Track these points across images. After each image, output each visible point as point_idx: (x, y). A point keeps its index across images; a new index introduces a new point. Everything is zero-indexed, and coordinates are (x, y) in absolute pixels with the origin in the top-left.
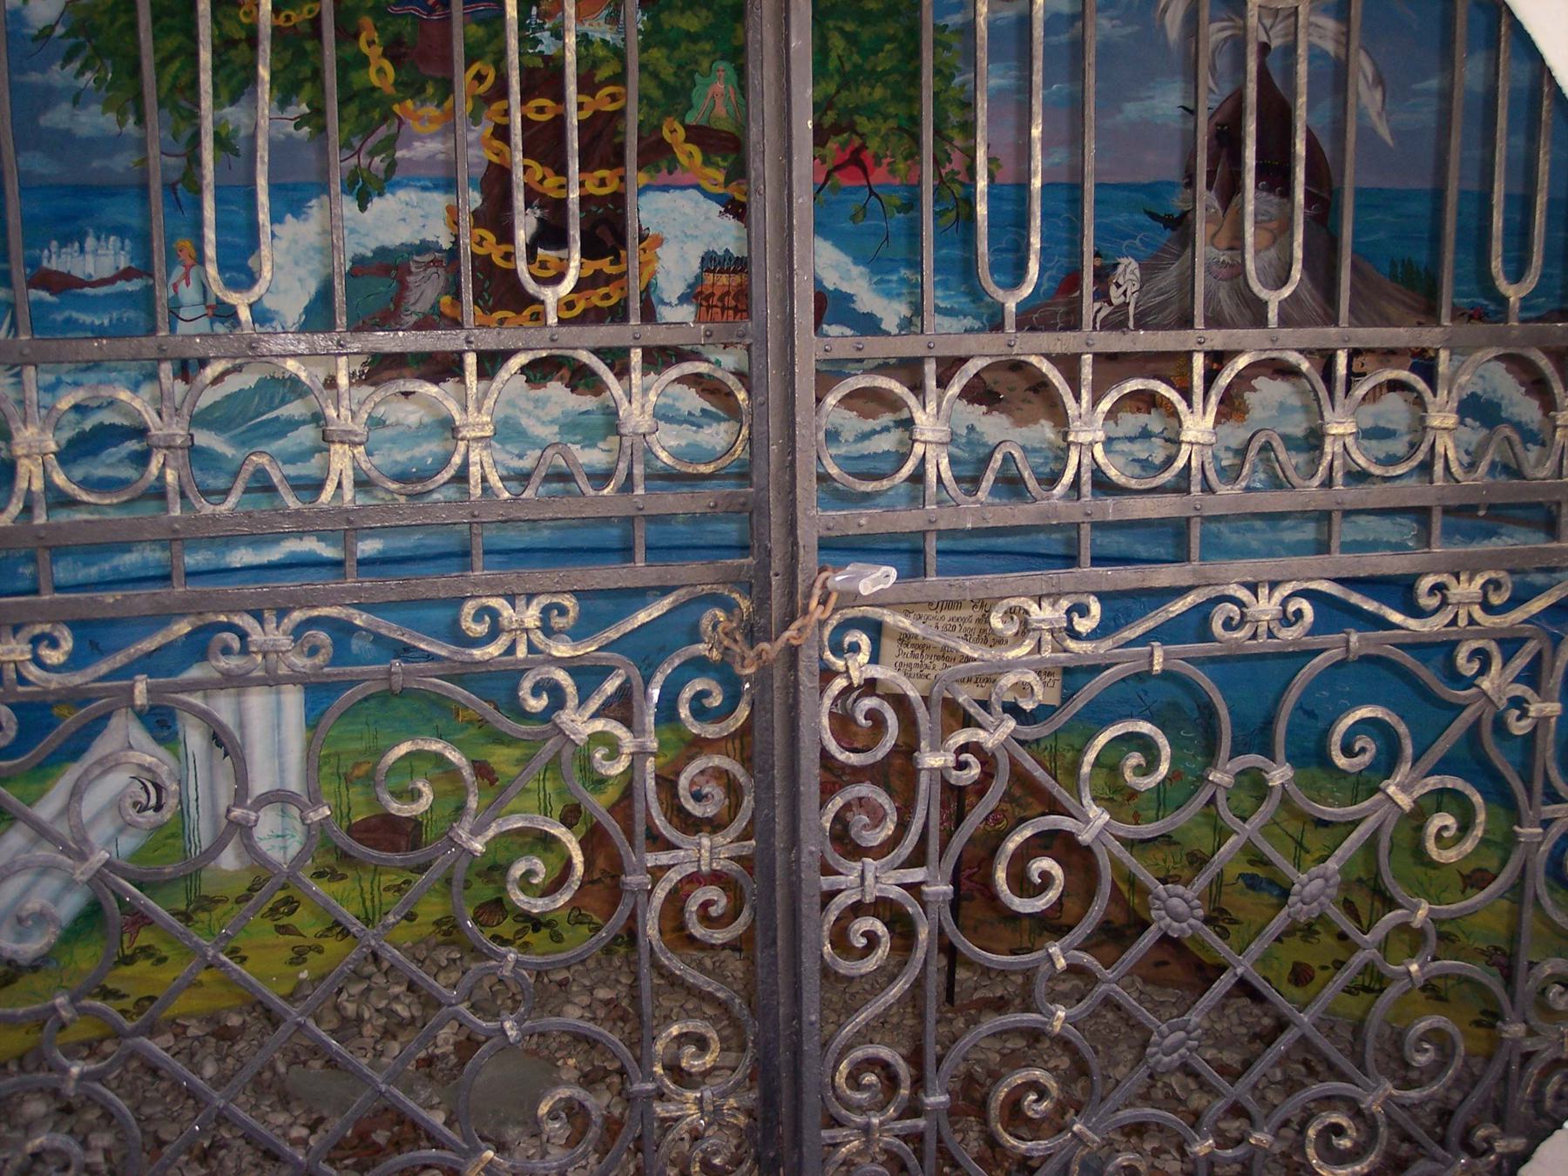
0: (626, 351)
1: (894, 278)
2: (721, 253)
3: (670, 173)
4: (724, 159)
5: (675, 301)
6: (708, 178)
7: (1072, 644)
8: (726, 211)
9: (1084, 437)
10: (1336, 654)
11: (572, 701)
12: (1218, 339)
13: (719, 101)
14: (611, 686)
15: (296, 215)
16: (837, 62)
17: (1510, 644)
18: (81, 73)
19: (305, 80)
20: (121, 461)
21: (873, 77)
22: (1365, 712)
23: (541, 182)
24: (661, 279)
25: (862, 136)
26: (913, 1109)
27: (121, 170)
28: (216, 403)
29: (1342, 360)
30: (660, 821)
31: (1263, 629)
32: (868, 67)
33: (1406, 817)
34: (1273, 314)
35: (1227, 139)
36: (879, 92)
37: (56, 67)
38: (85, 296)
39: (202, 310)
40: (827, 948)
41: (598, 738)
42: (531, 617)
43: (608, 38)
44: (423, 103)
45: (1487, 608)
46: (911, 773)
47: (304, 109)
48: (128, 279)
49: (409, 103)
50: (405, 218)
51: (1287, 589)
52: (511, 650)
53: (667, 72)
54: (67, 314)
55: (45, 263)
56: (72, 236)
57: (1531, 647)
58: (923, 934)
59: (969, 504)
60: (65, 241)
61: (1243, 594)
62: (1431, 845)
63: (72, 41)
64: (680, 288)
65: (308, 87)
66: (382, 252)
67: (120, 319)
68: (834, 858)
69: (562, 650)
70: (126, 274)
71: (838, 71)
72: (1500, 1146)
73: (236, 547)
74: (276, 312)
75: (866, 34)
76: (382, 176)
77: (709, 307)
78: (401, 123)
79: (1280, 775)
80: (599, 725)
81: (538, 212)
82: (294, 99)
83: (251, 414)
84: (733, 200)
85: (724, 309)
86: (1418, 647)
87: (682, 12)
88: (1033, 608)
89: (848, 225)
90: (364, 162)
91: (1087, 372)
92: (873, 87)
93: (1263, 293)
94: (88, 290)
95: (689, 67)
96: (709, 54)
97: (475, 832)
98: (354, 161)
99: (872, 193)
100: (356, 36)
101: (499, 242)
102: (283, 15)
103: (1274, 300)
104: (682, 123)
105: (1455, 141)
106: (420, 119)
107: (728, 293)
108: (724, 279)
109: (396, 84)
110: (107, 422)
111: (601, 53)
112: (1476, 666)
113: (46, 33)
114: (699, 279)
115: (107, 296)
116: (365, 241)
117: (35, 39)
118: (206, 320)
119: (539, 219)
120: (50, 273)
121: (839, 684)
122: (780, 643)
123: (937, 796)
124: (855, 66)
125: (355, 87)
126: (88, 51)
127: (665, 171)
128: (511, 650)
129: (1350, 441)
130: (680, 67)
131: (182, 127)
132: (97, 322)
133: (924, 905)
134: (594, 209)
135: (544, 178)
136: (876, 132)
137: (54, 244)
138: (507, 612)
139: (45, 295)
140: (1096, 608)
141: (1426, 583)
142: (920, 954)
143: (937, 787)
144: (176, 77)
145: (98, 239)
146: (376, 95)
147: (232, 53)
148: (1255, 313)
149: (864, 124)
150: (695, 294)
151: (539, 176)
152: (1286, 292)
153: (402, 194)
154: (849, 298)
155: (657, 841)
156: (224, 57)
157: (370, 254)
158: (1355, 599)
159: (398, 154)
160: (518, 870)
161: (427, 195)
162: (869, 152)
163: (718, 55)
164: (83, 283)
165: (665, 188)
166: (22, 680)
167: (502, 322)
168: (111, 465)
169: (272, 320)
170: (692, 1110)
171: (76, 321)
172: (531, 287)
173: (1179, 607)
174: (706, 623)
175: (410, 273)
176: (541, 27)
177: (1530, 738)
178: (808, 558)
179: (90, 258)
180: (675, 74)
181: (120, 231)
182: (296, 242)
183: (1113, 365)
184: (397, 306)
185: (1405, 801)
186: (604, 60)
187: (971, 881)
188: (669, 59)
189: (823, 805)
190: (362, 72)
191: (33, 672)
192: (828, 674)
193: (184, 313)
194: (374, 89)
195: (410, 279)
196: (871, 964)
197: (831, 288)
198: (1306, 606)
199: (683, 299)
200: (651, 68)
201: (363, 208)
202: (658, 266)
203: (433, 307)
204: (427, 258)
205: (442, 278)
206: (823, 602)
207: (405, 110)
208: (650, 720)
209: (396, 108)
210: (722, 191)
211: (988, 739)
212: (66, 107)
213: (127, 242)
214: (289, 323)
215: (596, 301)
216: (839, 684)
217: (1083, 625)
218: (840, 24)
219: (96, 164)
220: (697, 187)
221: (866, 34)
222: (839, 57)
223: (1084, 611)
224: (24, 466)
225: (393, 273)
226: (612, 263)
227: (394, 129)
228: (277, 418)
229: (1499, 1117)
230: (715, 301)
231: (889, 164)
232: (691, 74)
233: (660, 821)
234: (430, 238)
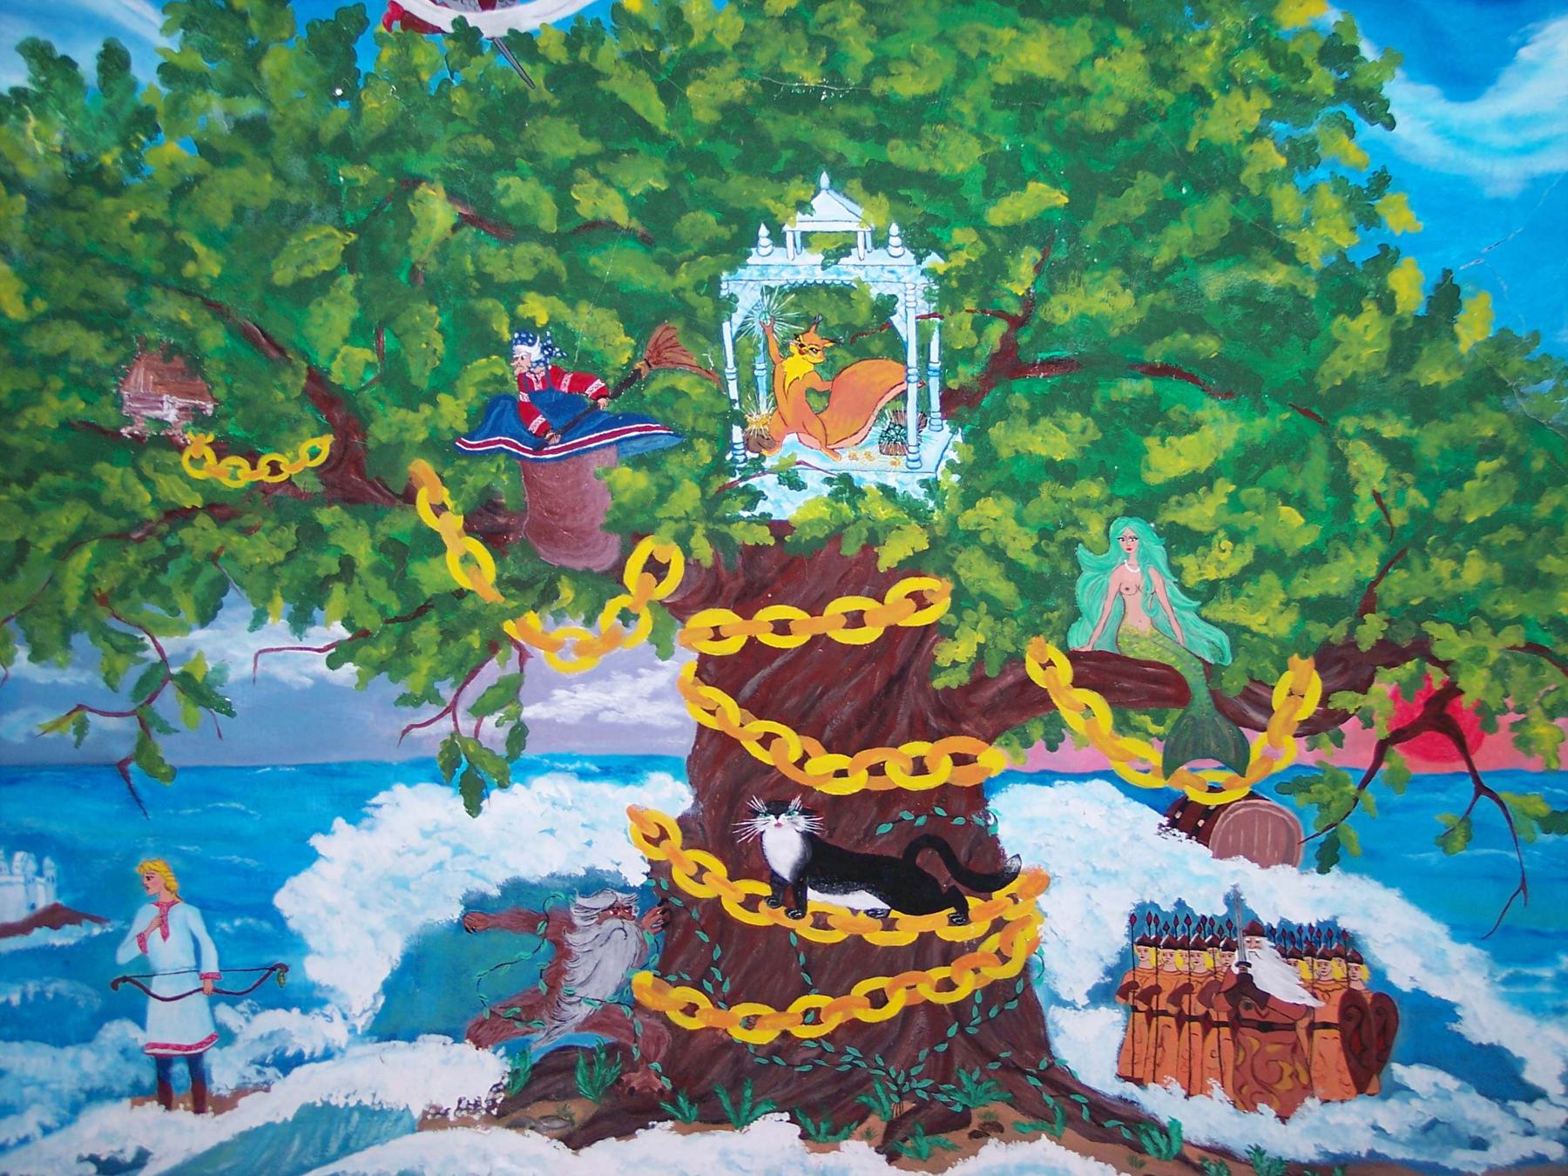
1: (1547, 973)
2: (1167, 907)
3: (1052, 747)
4: (1159, 721)
5: (1082, 1000)
6: (1129, 758)
8: (1174, 824)
13: (1135, 601)
15: (354, 818)
16: (1373, 507)
19: (329, 579)
21: (1459, 536)
23: (800, 764)
24: (1052, 956)
25: (1445, 665)
27: (19, 739)
32: (1444, 514)
36: (1475, 570)
39: (191, 983)
43: (891, 483)
44: (559, 616)
47: (340, 632)
48: (55, 926)
49: (532, 618)
53: (1021, 546)
64: (1092, 975)
65: (338, 589)
66: (516, 888)
67: (40, 995)
70: (53, 917)
71: (1378, 527)
74: (332, 990)
75: (1431, 442)
76: (502, 751)
77: (1151, 1015)
78: (524, 656)
81: (802, 823)
82: (316, 612)
84: (1184, 804)
85: (1182, 1019)
87: (1033, 420)
89: (1434, 857)
90: (467, 725)
92: (1460, 559)
95: (1061, 535)
96: (1098, 505)
98: (446, 724)
99: (1481, 789)
100: (409, 497)
101: (733, 876)
102: (263, 463)
104: (1063, 647)
106: (555, 647)
107: (1187, 988)
108: (1178, 960)
109: (500, 583)
114: (1127, 959)
116: (481, 867)
118: (200, 1000)
119: (807, 837)
124: (1414, 513)
125: (428, 592)
127: (1040, 743)
130: (1045, 534)
134: (907, 816)
135: (805, 757)
136: (1477, 657)
144: (90, 579)
146: (468, 604)
147: (186, 534)
149: (1447, 640)
150: (1122, 987)
151: (795, 755)
153: (544, 785)
154: (1447, 1010)
156: (172, 541)
157: (495, 892)
159: (528, 713)
161: (589, 786)
162: (1467, 701)
163: (1118, 507)
165: (1045, 777)
169: (323, 1002)
175: (573, 928)
176: (757, 467)
180: (1037, 550)
184: (553, 987)
186: (890, 527)
188: (1020, 521)
190: (434, 562)
193: (159, 986)
194: (461, 594)
195: (573, 938)
197: (1406, 987)
199: (1099, 996)
200: (986, 539)
201: (474, 808)
202: (1042, 929)
203: (619, 990)
204: (602, 901)
205: (633, 939)
207: (525, 629)
209: (509, 627)
210: (1160, 783)
213: (47, 862)
214: (357, 1010)
215: (926, 992)
218: (1370, 423)
220: (1108, 775)
221: (1431, 442)
222: (1377, 496)
225: (542, 927)
226: (952, 922)
227: (512, 667)
230: (1162, 1002)
231: (1515, 726)
232: (1070, 546)
234: (604, 866)
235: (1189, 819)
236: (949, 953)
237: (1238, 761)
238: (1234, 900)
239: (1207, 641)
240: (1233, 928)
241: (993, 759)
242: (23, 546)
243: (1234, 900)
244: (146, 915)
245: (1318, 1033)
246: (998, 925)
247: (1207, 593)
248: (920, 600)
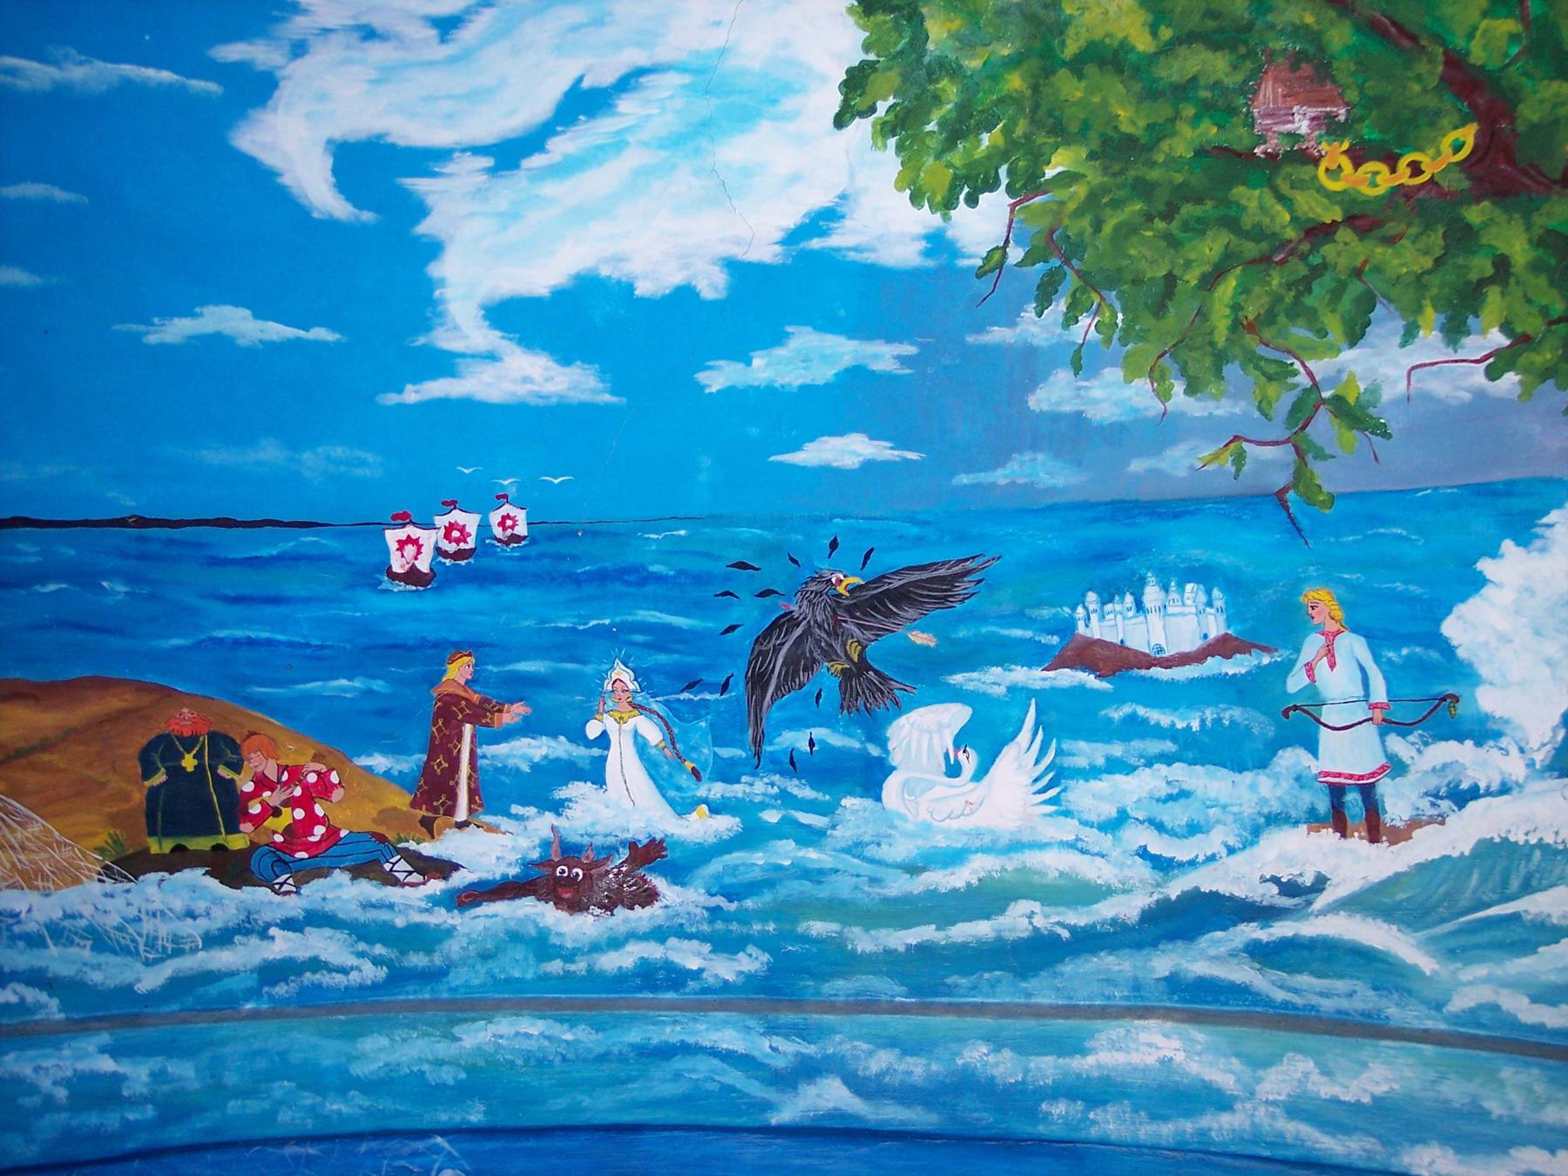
18: (1070, 319)
19: (1483, 282)
20: (1233, 954)
27: (1182, 473)
28: (1398, 875)
37: (1029, 312)
38: (1155, 681)
39: (1361, 712)
48: (1227, 656)
54: (1127, 709)
55: (1081, 629)
56: (1120, 585)
60: (1109, 594)
63: (1040, 267)
65: (1493, 295)
70: (1224, 647)
73: (1423, 1141)
74: (1507, 722)
83: (1464, 902)
94: (1156, 672)
102: (1403, 163)
105: (266, 552)
110: (1205, 889)
113: (995, 262)
115: (1192, 681)
117: (980, 273)
118: (1369, 730)
120: (1092, 643)
126: (1071, 281)
131: (1272, 390)
132: (1180, 725)
137: (1092, 597)
139: (1089, 679)
144: (1236, 307)
145: (1166, 589)
147: (1328, 250)
156: (1315, 260)
164: (1149, 662)
168: (1215, 958)
169: (1498, 735)
171: (1145, 721)
179: (1153, 618)
181: (1203, 575)
182: (1530, 591)
193: (1329, 715)
212: (1064, 376)
213: (1216, 592)
214: (1534, 744)
219: (1137, 466)
228: (1516, 917)
242: (1171, 280)
244: (1313, 645)
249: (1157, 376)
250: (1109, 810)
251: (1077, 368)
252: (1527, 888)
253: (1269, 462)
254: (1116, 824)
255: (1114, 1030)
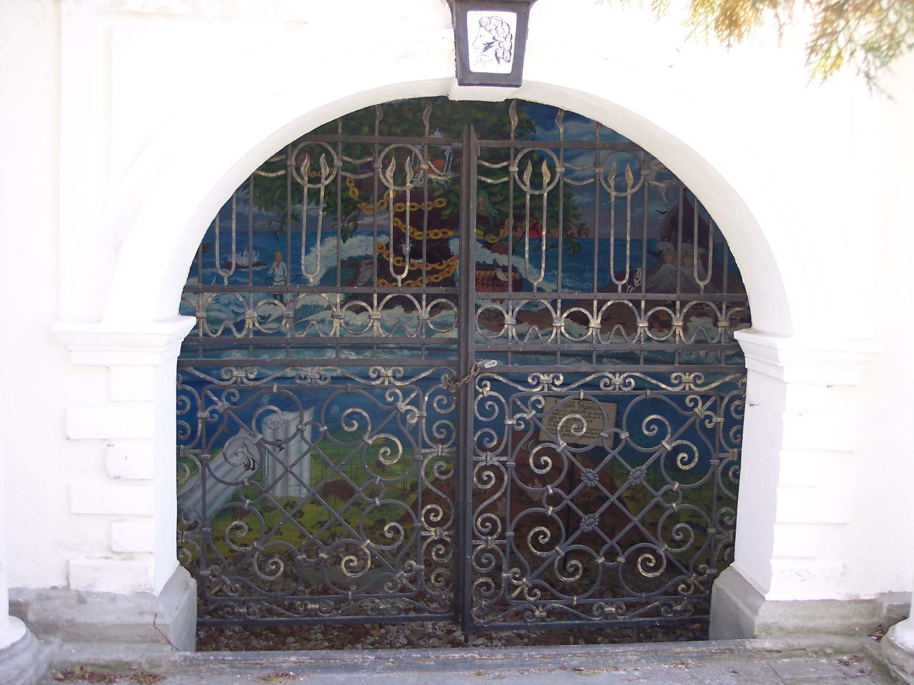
0: (421, 295)
7: (554, 388)
9: (558, 325)
10: (643, 397)
11: (401, 400)
12: (601, 296)
14: (413, 395)
17: (705, 397)
22: (654, 417)
26: (502, 536)
29: (643, 303)
30: (426, 439)
31: (617, 387)
33: (669, 453)
34: (620, 288)
35: (673, 222)
40: (475, 479)
41: (408, 411)
42: (390, 373)
45: (696, 385)
46: (503, 425)
49: (364, 204)
50: (358, 246)
51: (625, 375)
52: (383, 382)
57: (713, 399)
58: (506, 478)
59: (521, 343)
61: (611, 376)
62: (679, 463)
66: (351, 258)
68: (478, 451)
69: (398, 384)
70: (257, 264)
72: (708, 571)
78: (360, 210)
79: (624, 435)
80: (409, 407)
84: (486, 242)
85: (483, 284)
86: (672, 396)
88: (542, 376)
90: (346, 225)
91: (559, 305)
93: (617, 282)
97: (370, 438)
103: (620, 284)
106: (368, 210)
111: (436, 186)
112: (692, 404)
121: (481, 396)
122: (462, 382)
123: (511, 434)
128: (383, 382)
129: (646, 329)
133: (506, 468)
138: (383, 371)
140: (562, 378)
141: (674, 375)
142: (505, 484)
143: (511, 431)
148: (613, 289)
152: (624, 282)
153: (359, 237)
155: (426, 446)
158: (649, 379)
160: (382, 451)
166: (242, 382)
167: (383, 284)
170: (433, 534)
172: (394, 275)
173: (588, 379)
174: (443, 378)
177: (714, 429)
178: (472, 357)
183: (566, 305)
184: (356, 279)
185: (669, 447)
187: (522, 465)
189: (474, 434)
191: (245, 381)
192: (477, 393)
193: (276, 279)
196: (489, 486)
198: (632, 381)
201: (344, 242)
204: (367, 261)
206: (475, 370)
208: (424, 407)
211: (527, 416)
215: (432, 280)
216: (481, 396)
217: (557, 383)
223: (558, 379)
224: (248, 321)
229: (708, 562)
233: (426, 439)
235: (487, 245)
236: (438, 272)
237: (497, 235)
238: (495, 261)
239: (494, 212)
240: (495, 266)
241: (451, 233)
242: (270, 188)
243: (495, 261)
244: (275, 264)
245: (476, 66)
246: (448, 266)
247: (495, 204)
248: (441, 203)
249: (260, 207)
250: (227, 301)
251: (245, 203)
252: (311, 314)
253: (276, 224)
254: (227, 305)
255: (227, 353)
